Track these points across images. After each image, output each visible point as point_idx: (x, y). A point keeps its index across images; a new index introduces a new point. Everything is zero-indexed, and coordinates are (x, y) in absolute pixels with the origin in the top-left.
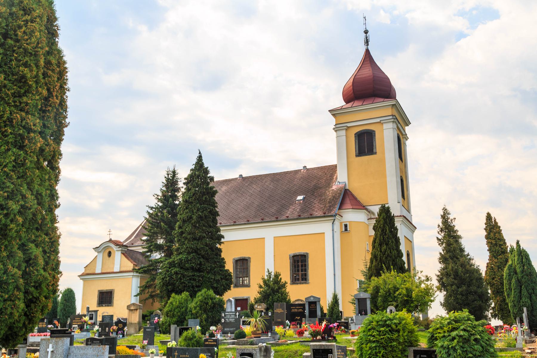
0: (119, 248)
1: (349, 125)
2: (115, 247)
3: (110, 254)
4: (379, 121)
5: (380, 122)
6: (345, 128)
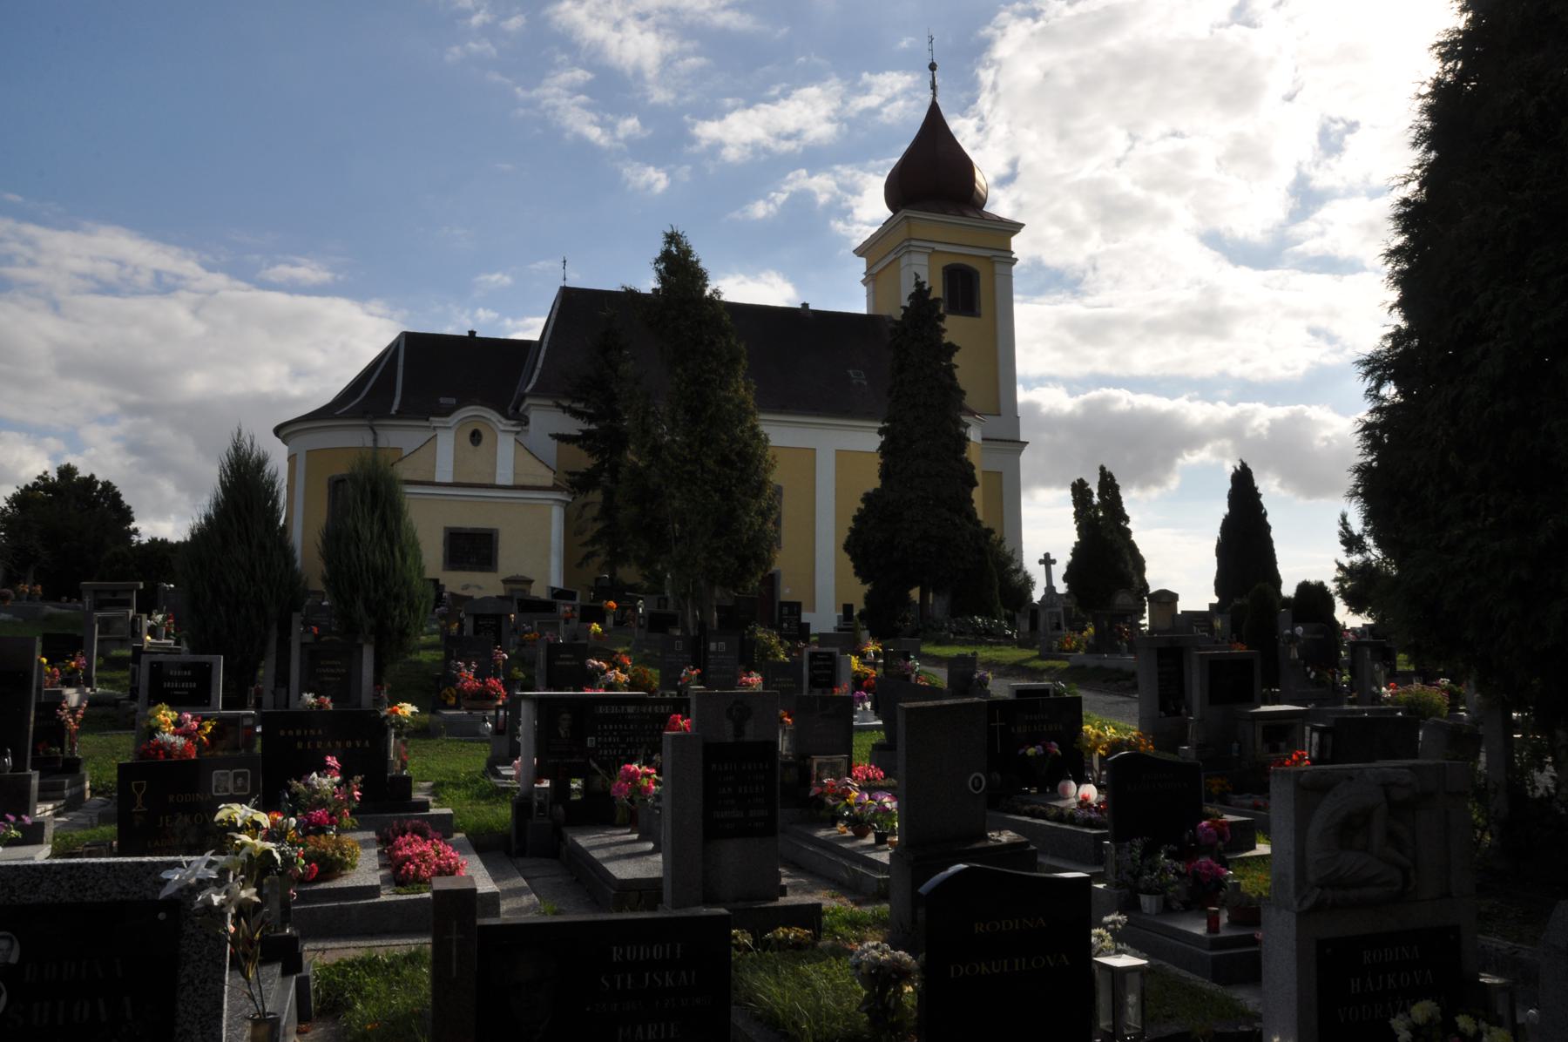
0: (513, 426)
1: (938, 247)
2: (504, 421)
3: (476, 437)
4: (989, 255)
5: (988, 258)
6: (930, 251)
